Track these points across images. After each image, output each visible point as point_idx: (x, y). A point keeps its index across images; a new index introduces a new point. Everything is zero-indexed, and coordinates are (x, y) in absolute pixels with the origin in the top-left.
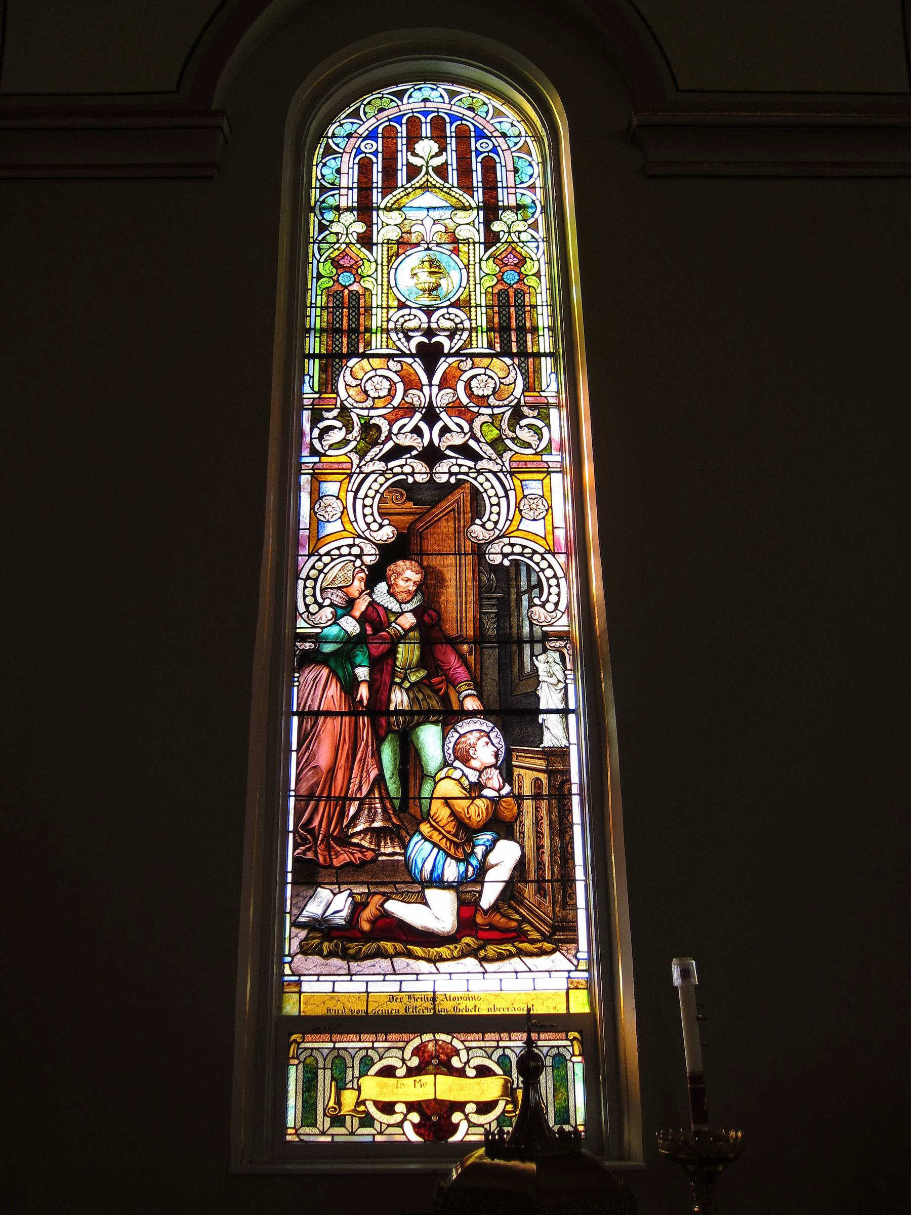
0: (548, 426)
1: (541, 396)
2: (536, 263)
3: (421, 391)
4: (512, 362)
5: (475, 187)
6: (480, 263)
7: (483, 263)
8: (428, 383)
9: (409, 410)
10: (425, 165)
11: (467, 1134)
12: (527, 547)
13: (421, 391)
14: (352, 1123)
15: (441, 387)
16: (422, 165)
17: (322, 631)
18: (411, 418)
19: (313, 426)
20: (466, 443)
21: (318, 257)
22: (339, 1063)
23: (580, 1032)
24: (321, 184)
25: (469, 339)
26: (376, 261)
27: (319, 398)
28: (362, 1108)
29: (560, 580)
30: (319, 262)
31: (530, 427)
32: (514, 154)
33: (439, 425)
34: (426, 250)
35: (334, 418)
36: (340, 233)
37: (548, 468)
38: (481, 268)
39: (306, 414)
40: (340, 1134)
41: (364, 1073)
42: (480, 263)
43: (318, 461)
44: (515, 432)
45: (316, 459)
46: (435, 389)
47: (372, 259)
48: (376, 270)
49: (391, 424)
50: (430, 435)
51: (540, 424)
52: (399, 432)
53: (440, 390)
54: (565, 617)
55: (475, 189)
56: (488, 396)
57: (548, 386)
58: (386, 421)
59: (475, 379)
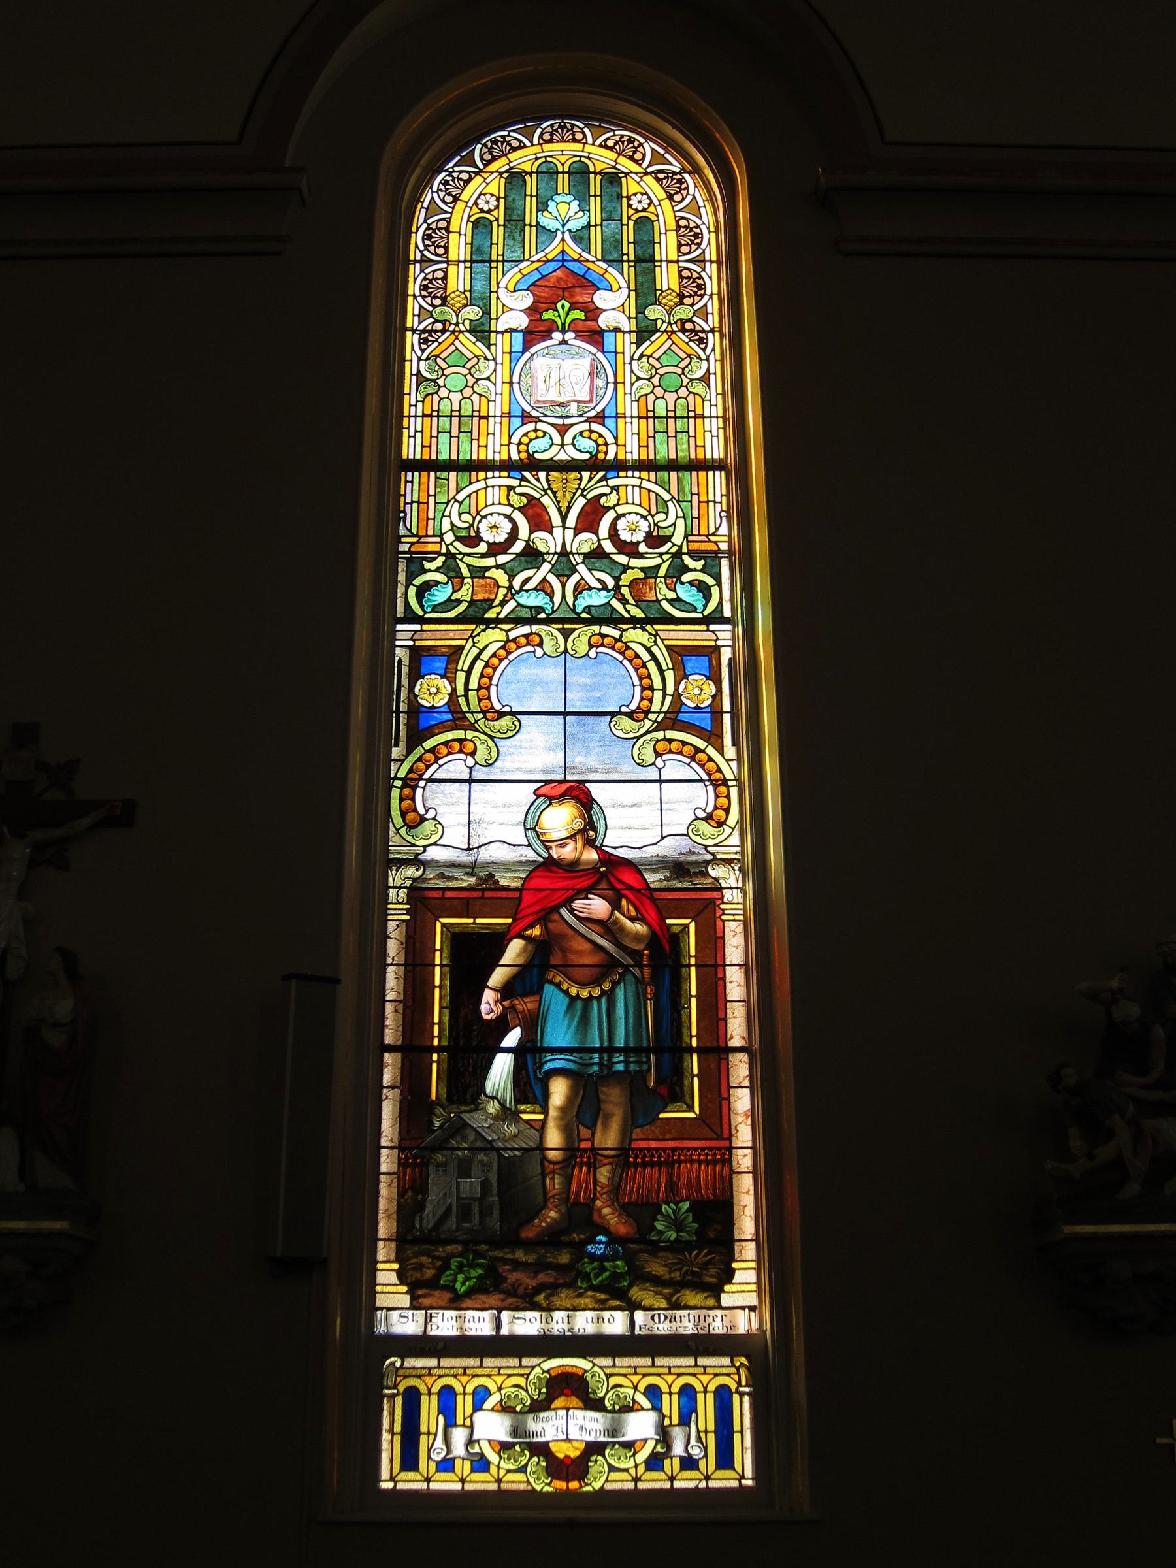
0: (719, 584)
1: (710, 541)
2: (704, 364)
3: (551, 533)
4: (670, 497)
5: (658, 261)
7: (634, 363)
8: (561, 524)
9: (532, 556)
10: (561, 229)
11: (607, 1480)
12: (713, 761)
13: (551, 533)
14: (463, 1468)
15: (577, 531)
16: (557, 230)
17: (424, 851)
18: (538, 568)
19: (409, 583)
21: (419, 353)
22: (447, 1397)
23: (747, 1357)
24: (423, 255)
25: (667, 487)
26: (494, 360)
27: (418, 542)
28: (476, 1449)
29: (730, 789)
30: (419, 359)
32: (677, 214)
33: (575, 578)
34: (560, 343)
35: (437, 570)
36: (449, 321)
37: (716, 640)
38: (632, 371)
39: (402, 566)
41: (478, 1407)
42: (630, 363)
43: (419, 629)
44: (675, 590)
46: (569, 534)
47: (490, 357)
49: (511, 577)
51: (710, 581)
52: (521, 590)
53: (575, 535)
54: (737, 833)
55: (500, 258)
56: (638, 543)
58: (506, 575)
59: (623, 519)
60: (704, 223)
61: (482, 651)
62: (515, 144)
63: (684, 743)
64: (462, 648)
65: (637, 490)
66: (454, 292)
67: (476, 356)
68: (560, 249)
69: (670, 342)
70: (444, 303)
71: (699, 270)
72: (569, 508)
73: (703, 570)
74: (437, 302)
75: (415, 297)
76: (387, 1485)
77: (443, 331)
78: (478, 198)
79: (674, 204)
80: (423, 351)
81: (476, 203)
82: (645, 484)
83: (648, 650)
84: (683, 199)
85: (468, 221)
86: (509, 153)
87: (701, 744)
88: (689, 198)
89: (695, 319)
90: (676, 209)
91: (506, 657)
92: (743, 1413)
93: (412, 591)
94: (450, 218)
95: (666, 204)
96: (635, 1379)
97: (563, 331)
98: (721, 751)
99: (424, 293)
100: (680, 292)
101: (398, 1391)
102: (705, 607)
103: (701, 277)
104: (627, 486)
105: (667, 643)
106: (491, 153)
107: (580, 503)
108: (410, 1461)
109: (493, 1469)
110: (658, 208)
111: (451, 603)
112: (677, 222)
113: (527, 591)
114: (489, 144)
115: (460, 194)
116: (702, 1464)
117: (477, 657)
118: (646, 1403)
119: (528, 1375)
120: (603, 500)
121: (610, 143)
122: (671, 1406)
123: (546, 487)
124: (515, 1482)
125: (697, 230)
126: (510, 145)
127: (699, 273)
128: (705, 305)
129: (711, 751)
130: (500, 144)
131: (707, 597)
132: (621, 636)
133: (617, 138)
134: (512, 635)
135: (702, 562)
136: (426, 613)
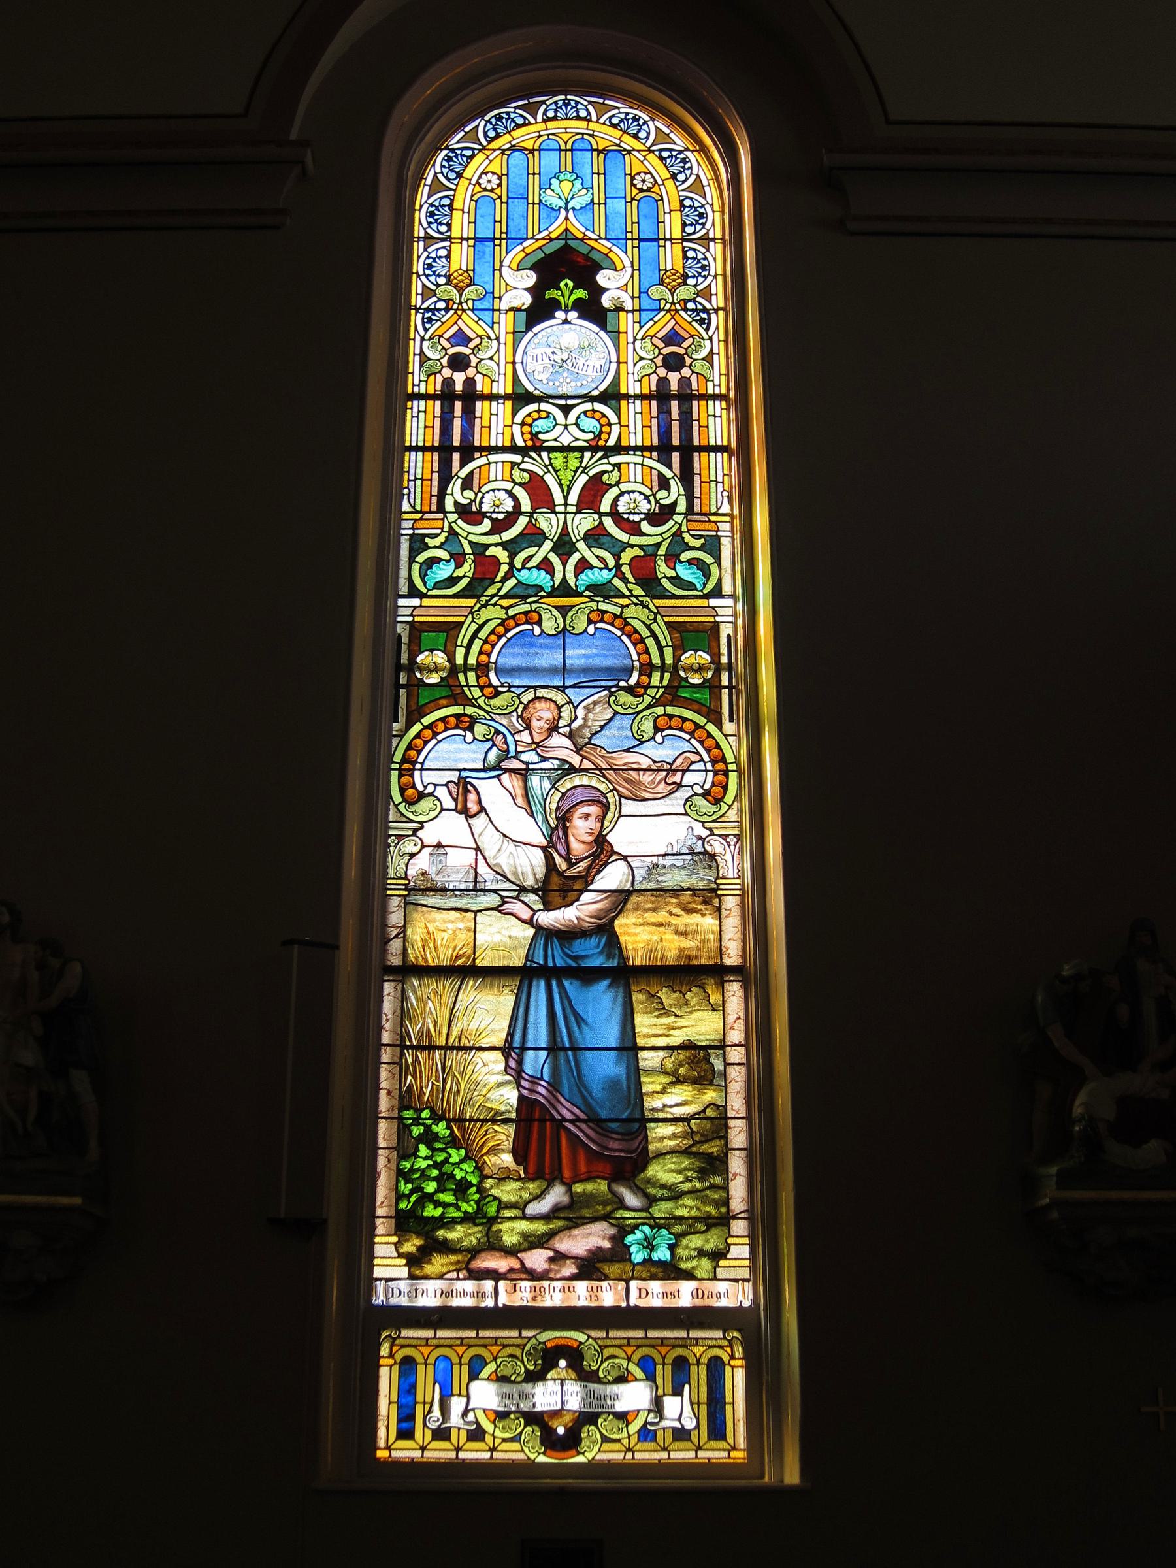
0: (718, 561)
6: (634, 343)
9: (534, 536)
16: (560, 208)
18: (540, 546)
20: (610, 582)
24: (426, 233)
27: (421, 519)
30: (423, 339)
31: (690, 562)
32: (681, 193)
33: (576, 557)
40: (440, 1452)
41: (474, 1376)
42: (634, 343)
44: (674, 569)
45: (416, 602)
48: (498, 350)
49: (512, 556)
50: (565, 571)
52: (523, 567)
57: (718, 509)
60: (708, 203)
61: (481, 627)
62: (520, 121)
63: (684, 719)
64: (462, 623)
65: (639, 467)
66: (457, 271)
67: (478, 336)
68: (563, 228)
69: (673, 322)
70: (449, 283)
71: (703, 250)
72: (569, 490)
73: (702, 548)
74: (442, 280)
75: (418, 276)
76: (382, 1454)
77: (447, 310)
78: (480, 177)
79: (678, 184)
80: (426, 330)
81: (478, 183)
82: (647, 462)
83: (648, 627)
84: (687, 179)
85: (471, 200)
86: (513, 130)
87: (701, 720)
88: (693, 178)
89: (699, 299)
90: (679, 188)
91: (504, 635)
92: (736, 1381)
93: (416, 567)
94: (454, 196)
95: (670, 184)
96: (629, 1350)
97: (567, 311)
98: (719, 726)
99: (428, 272)
100: (684, 272)
101: (395, 1361)
102: (705, 585)
103: (705, 258)
104: (628, 463)
105: (666, 619)
106: (495, 130)
107: (583, 479)
108: (406, 1433)
109: (489, 1438)
110: (662, 187)
111: (452, 581)
112: (682, 202)
113: (529, 569)
114: (493, 121)
115: (464, 170)
116: (694, 1435)
117: (475, 636)
118: (639, 1374)
119: (525, 1346)
120: (605, 477)
121: (615, 121)
122: (662, 1373)
123: (547, 463)
124: (510, 1453)
125: (702, 210)
126: (514, 122)
127: (704, 254)
128: (710, 285)
129: (711, 727)
130: (504, 121)
131: (707, 575)
132: (622, 612)
133: (622, 116)
134: (511, 612)
135: (702, 541)
136: (428, 590)
